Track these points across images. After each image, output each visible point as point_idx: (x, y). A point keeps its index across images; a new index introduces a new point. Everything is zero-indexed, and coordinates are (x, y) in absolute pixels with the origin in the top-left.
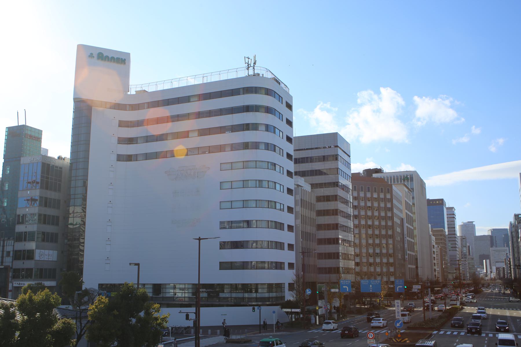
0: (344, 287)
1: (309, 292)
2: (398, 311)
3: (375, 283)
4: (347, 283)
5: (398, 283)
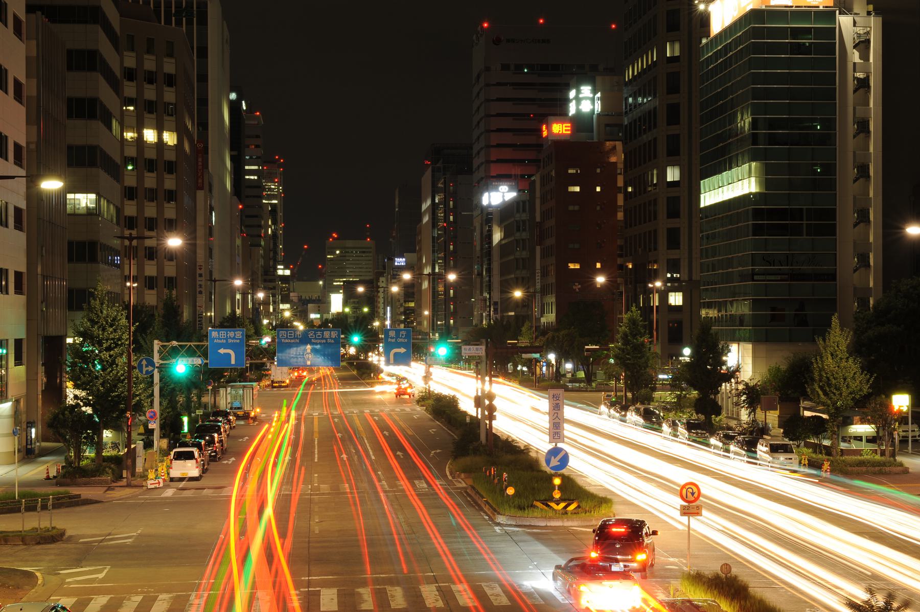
0: (222, 351)
1: (147, 366)
3: (323, 338)
4: (234, 338)
5: (393, 340)
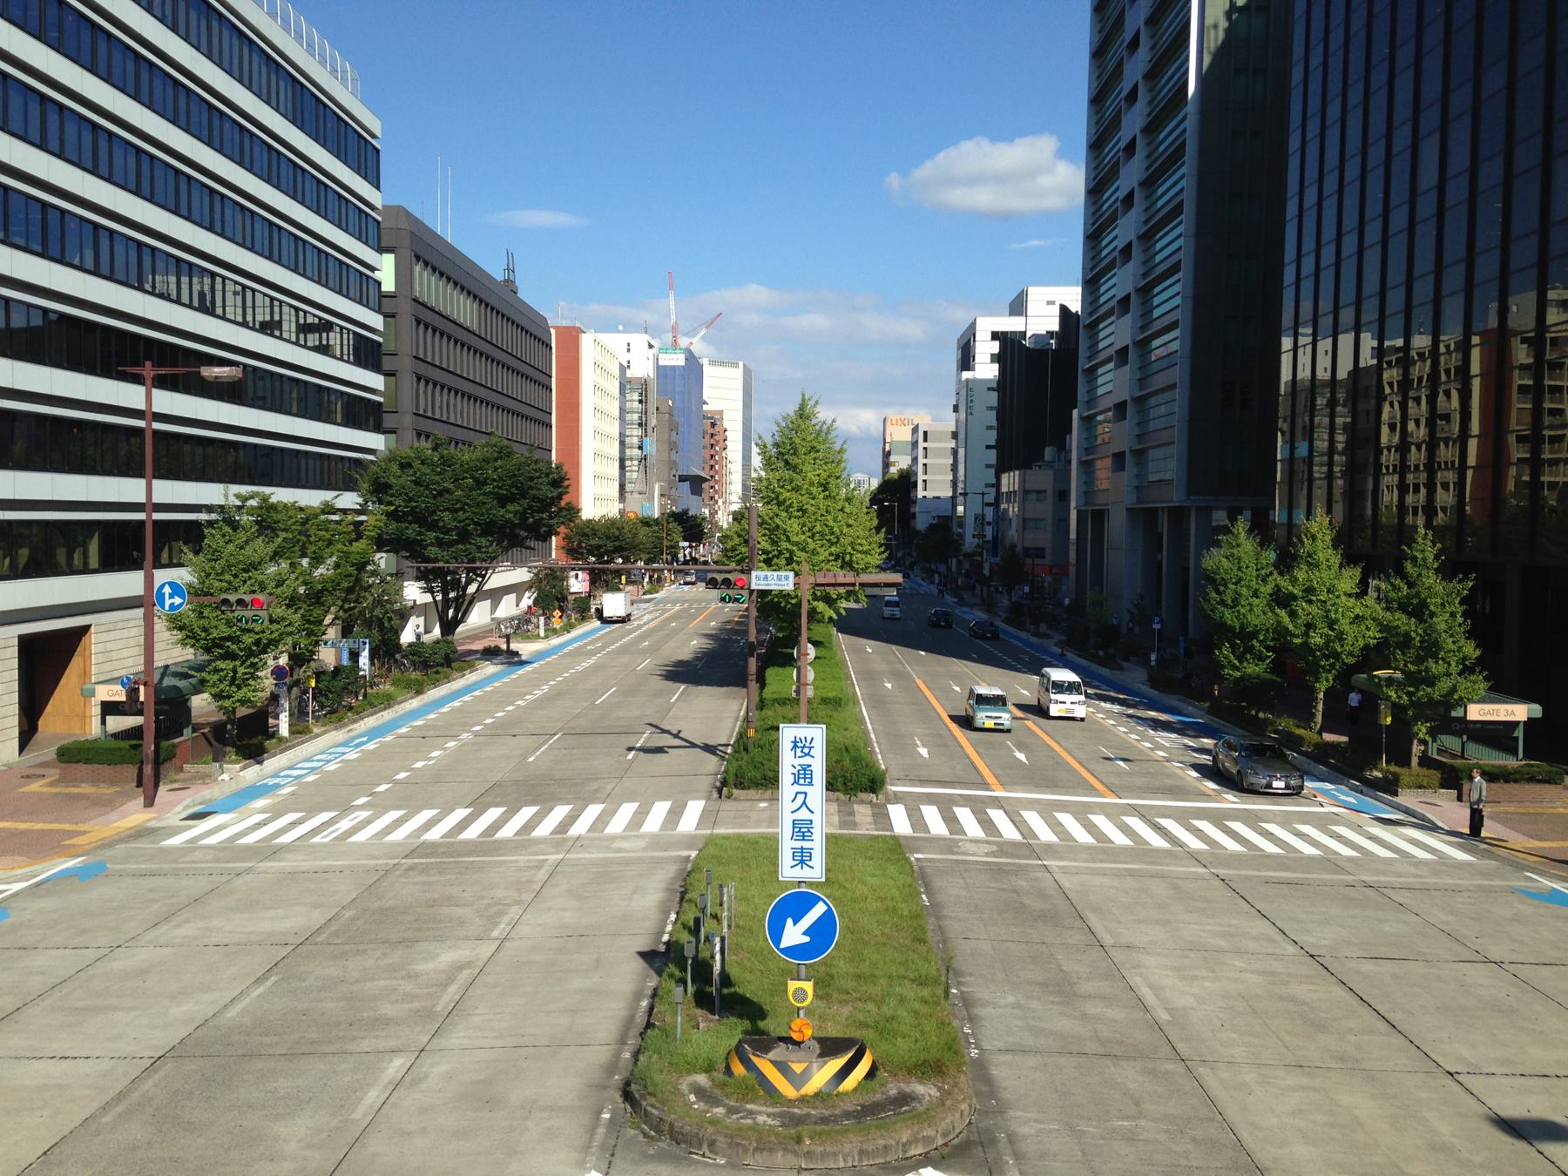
1: (171, 596)
2: (803, 814)
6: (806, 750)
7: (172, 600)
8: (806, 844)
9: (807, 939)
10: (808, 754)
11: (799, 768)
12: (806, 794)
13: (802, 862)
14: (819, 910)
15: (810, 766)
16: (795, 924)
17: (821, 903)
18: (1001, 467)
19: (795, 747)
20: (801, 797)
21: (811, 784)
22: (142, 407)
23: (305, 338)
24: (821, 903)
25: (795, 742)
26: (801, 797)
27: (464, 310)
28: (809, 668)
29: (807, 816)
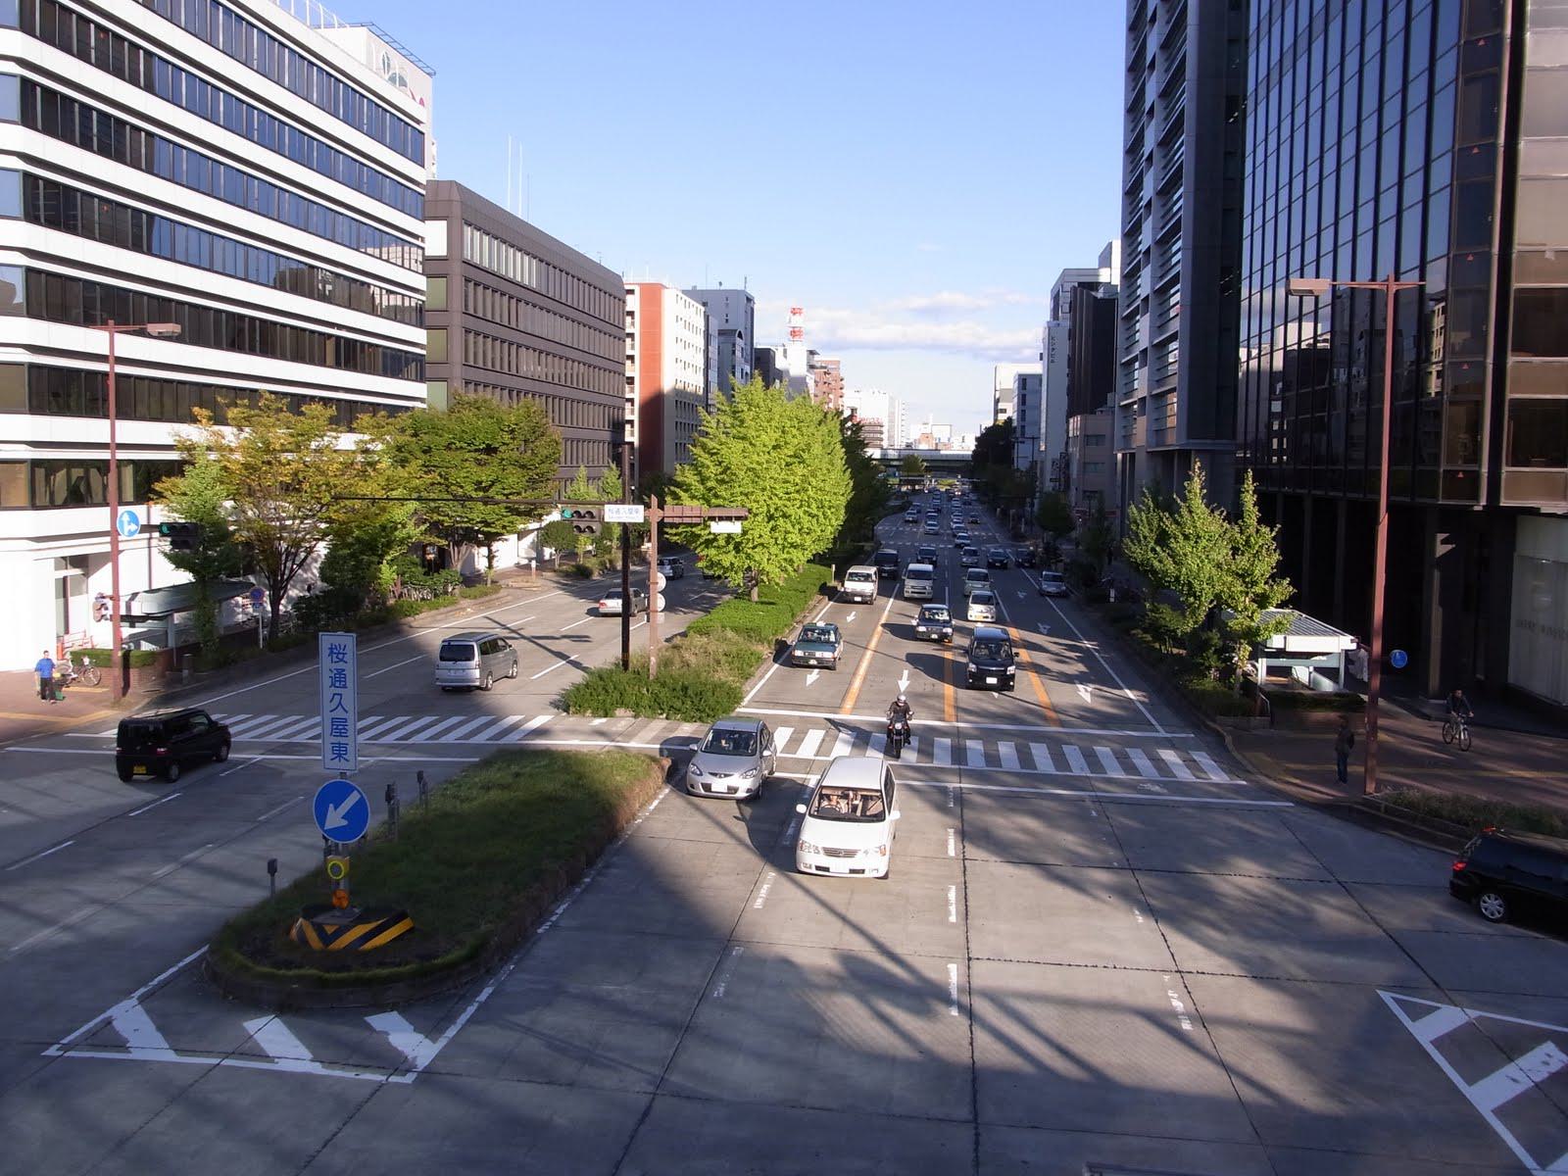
1: (129, 523)
2: (339, 713)
6: (341, 656)
7: (130, 527)
8: (342, 740)
9: (344, 823)
10: (342, 660)
11: (335, 672)
12: (341, 695)
13: (340, 756)
14: (354, 798)
15: (344, 670)
16: (336, 808)
17: (355, 792)
18: (1070, 414)
19: (332, 653)
20: (337, 698)
21: (345, 687)
22: (106, 352)
23: (403, 303)
24: (355, 792)
25: (331, 649)
26: (337, 698)
27: (521, 268)
28: (660, 595)
29: (344, 715)
